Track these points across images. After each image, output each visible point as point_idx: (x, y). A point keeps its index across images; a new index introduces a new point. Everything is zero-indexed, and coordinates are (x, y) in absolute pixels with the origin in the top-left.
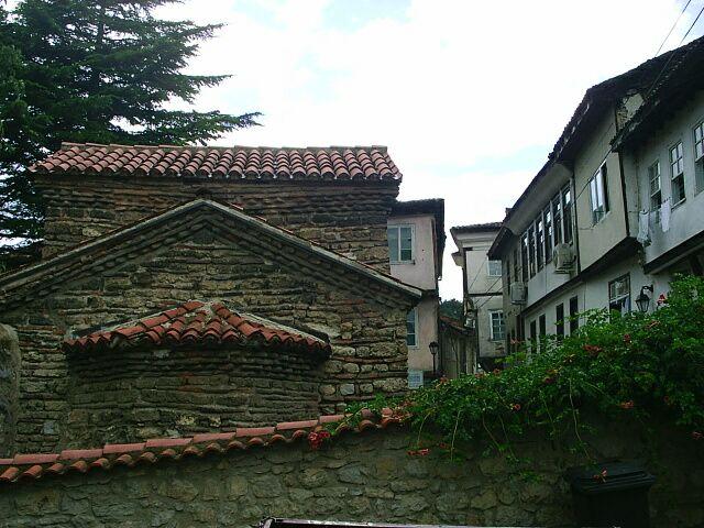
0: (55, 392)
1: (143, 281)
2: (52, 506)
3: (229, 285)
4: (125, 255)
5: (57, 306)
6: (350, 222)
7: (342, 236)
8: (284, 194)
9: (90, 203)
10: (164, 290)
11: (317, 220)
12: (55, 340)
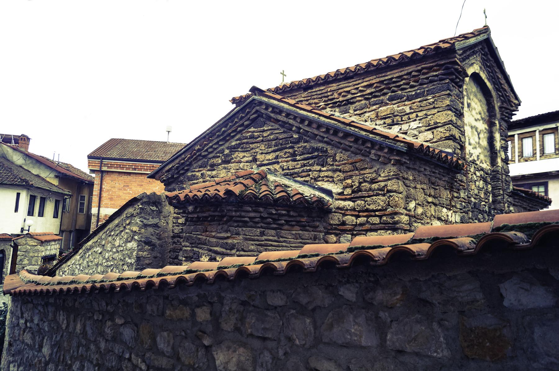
3: (271, 156)
4: (217, 143)
6: (417, 96)
7: (411, 108)
8: (365, 84)
10: (237, 164)
11: (391, 99)
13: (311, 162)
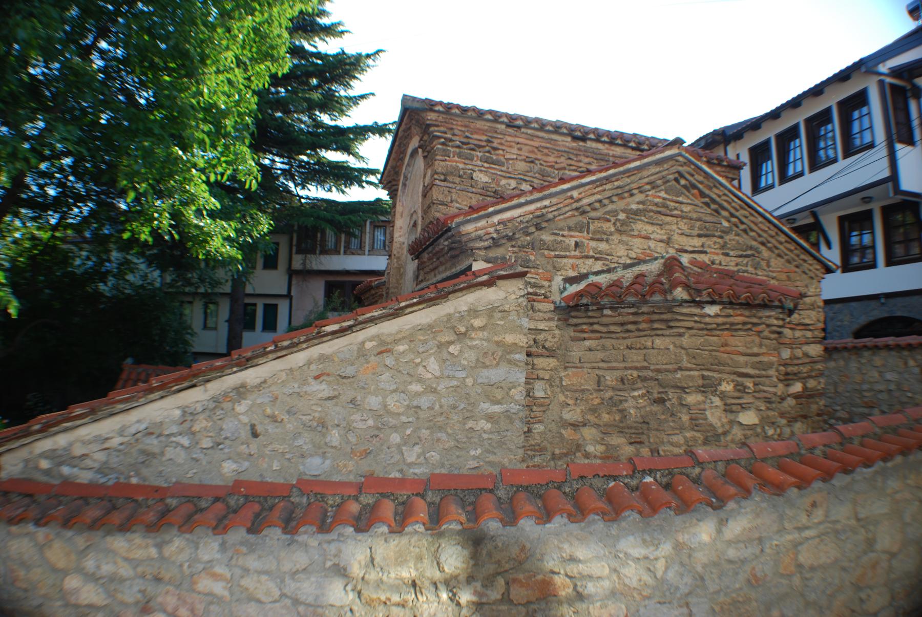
0: (544, 347)
2: (819, 514)
5: (544, 246)
9: (480, 147)
12: (542, 287)
13: (745, 260)
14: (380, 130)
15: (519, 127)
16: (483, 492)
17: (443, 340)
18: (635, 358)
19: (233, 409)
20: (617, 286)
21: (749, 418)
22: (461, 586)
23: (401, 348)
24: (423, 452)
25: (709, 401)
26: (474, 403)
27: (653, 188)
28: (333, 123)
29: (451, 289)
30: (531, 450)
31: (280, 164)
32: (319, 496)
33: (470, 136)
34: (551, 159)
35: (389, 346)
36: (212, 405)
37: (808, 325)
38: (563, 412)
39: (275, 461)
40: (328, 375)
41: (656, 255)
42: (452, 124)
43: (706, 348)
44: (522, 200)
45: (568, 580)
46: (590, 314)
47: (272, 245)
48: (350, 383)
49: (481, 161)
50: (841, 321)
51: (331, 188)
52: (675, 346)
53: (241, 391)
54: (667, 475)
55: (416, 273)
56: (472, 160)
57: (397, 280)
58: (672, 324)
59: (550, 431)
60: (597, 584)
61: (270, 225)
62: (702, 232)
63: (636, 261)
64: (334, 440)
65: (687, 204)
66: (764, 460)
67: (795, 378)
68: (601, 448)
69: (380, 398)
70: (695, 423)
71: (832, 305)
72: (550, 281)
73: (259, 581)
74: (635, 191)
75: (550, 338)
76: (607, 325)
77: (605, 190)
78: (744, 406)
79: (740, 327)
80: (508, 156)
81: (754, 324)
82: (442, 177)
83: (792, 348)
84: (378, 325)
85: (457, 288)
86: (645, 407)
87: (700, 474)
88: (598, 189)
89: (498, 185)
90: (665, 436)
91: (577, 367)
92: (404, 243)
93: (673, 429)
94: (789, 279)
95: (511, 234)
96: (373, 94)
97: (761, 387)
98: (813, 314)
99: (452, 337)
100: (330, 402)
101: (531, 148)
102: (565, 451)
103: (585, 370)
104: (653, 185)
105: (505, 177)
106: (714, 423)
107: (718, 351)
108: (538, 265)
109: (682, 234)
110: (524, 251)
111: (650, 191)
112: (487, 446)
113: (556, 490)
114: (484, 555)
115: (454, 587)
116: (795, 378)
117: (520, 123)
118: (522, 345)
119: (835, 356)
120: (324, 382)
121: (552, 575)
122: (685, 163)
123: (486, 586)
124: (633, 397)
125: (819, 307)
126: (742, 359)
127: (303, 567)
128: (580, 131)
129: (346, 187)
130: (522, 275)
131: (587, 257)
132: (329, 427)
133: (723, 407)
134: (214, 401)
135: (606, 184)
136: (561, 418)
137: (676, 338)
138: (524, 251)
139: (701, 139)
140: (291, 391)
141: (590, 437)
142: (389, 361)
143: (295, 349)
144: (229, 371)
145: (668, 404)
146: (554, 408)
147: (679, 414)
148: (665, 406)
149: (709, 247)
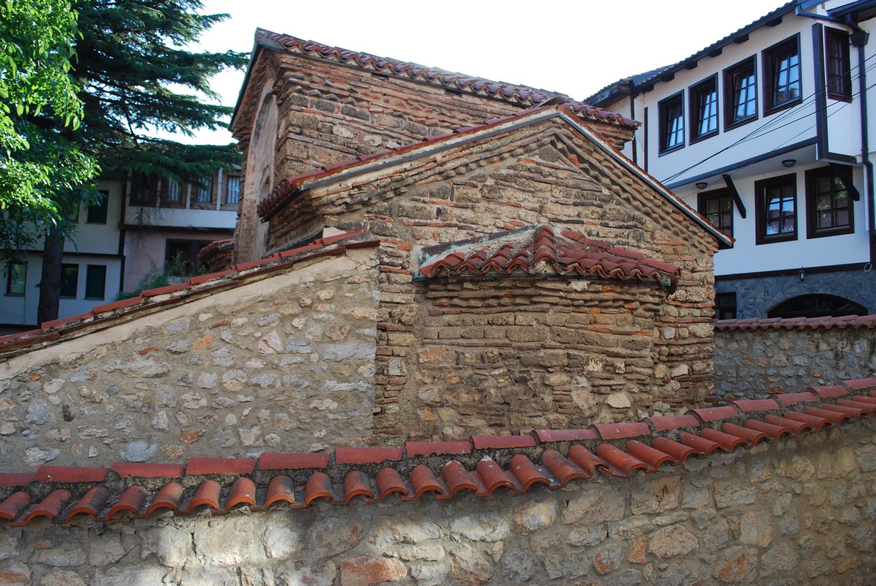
0: (400, 321)
1: (492, 195)
2: (671, 500)
5: (403, 213)
9: (342, 96)
12: (400, 257)
13: (626, 232)
14: (234, 60)
15: (386, 77)
16: (315, 471)
17: (286, 313)
18: (497, 334)
19: (42, 389)
20: (480, 258)
21: (620, 400)
22: (289, 572)
23: (239, 321)
24: (262, 434)
25: (574, 381)
26: (319, 381)
27: (526, 152)
28: (177, 48)
29: (296, 258)
30: (384, 432)
31: (109, 93)
32: (137, 480)
33: (331, 83)
34: (422, 114)
35: (227, 319)
36: (15, 385)
37: (696, 302)
38: (420, 392)
39: (92, 447)
40: (156, 350)
41: (526, 224)
42: (310, 69)
43: (572, 325)
44: (380, 162)
45: (402, 564)
46: (449, 287)
47: (99, 194)
48: (181, 359)
49: (342, 113)
50: (754, 298)
51: (174, 128)
52: (539, 323)
53: (53, 368)
54: (507, 454)
55: (267, 238)
56: (332, 111)
57: (247, 244)
58: (535, 299)
59: (405, 411)
60: (432, 568)
61: (97, 170)
62: (578, 201)
63: (504, 230)
64: (162, 421)
65: (564, 169)
66: (611, 441)
67: (680, 359)
68: (459, 430)
69: (215, 375)
70: (559, 405)
71: (744, 280)
72: (408, 250)
73: (65, 579)
74: (505, 155)
75: (407, 312)
76: (467, 299)
77: (472, 153)
78: (614, 387)
79: (610, 303)
80: (373, 109)
81: (627, 301)
82: (298, 130)
83: (677, 327)
84: (215, 296)
85: (302, 257)
86: (505, 387)
87: (541, 454)
88: (464, 152)
89: (361, 141)
90: (526, 418)
91: (435, 344)
92: (255, 201)
93: (535, 410)
94: (676, 252)
95: (366, 199)
96: (228, 15)
97: (633, 368)
98: (703, 291)
99: (297, 310)
100: (157, 379)
101: (399, 101)
102: (421, 434)
103: (444, 347)
104: (527, 148)
105: (369, 132)
106: (580, 406)
107: (585, 329)
108: (396, 233)
109: (557, 202)
110: (381, 218)
111: (522, 155)
112: (333, 428)
113: (391, 469)
114: (314, 538)
115: (282, 574)
116: (680, 359)
117: (387, 71)
118: (372, 318)
119: (737, 337)
120: (152, 358)
121: (385, 558)
122: (563, 125)
123: (316, 571)
124: (493, 376)
125: (709, 283)
126: (612, 337)
127: (116, 559)
128: (455, 83)
129: (193, 128)
130: (375, 244)
131: (450, 226)
132: (157, 408)
133: (590, 389)
134: (19, 381)
135: (473, 147)
136: (417, 397)
137: (540, 314)
138: (381, 218)
139: (605, 89)
140: (112, 368)
141: (448, 418)
142: (226, 335)
143: (118, 321)
144: (39, 346)
145: (530, 383)
146: (410, 387)
147: (542, 395)
148: (527, 385)
149: (586, 216)
